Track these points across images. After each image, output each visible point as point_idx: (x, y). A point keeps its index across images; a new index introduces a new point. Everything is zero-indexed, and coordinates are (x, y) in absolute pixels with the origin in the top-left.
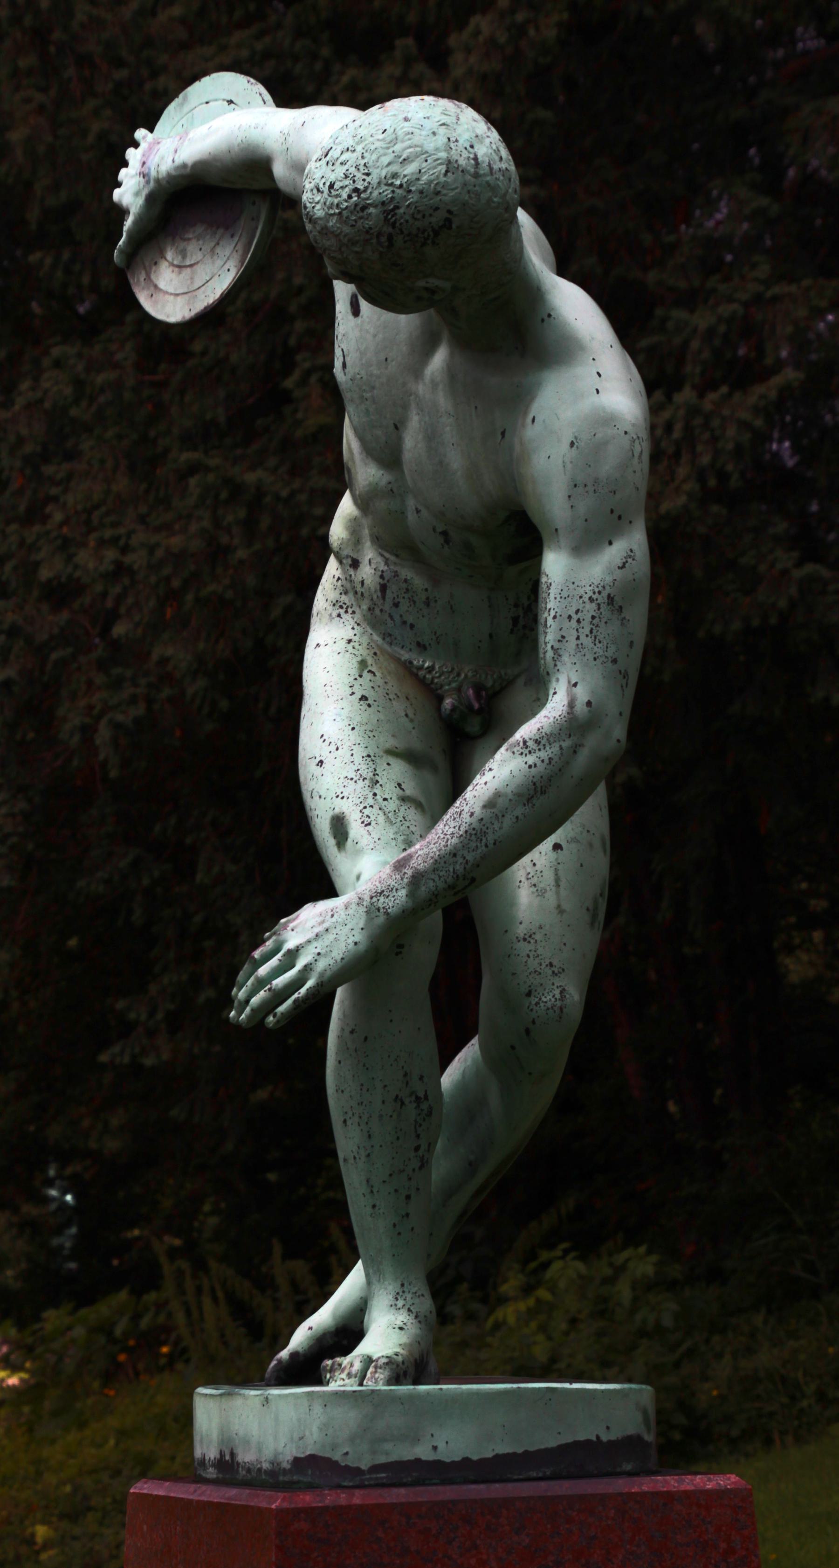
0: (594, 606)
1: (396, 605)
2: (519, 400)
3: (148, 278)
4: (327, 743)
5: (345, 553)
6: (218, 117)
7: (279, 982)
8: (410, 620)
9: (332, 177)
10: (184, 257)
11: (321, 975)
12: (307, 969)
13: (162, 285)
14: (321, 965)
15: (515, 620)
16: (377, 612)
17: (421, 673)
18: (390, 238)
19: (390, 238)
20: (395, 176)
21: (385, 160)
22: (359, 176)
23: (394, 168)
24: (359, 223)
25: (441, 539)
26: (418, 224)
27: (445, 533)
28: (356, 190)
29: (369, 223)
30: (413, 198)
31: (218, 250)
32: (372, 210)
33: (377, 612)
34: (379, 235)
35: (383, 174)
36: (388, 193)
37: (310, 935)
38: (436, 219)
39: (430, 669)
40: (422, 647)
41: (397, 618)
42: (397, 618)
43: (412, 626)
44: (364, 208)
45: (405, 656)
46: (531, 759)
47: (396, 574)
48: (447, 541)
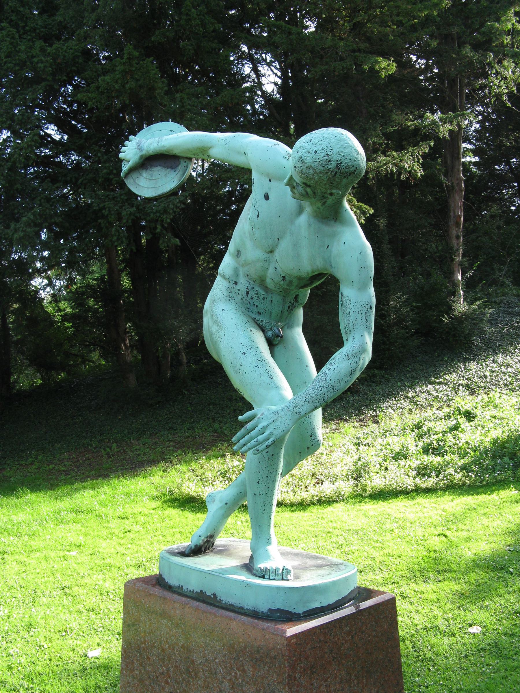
0: (366, 309)
1: (252, 299)
2: (334, 235)
3: (134, 181)
4: (245, 346)
5: (231, 279)
6: (166, 135)
7: (261, 438)
8: (257, 304)
9: (316, 149)
10: (152, 176)
11: (276, 436)
12: (271, 434)
13: (141, 184)
14: (276, 432)
15: (289, 307)
16: (244, 300)
17: (258, 322)
18: (336, 173)
19: (336, 173)
20: (342, 152)
21: (338, 146)
22: (328, 150)
23: (341, 149)
24: (326, 166)
25: (282, 279)
26: (347, 170)
27: (284, 277)
28: (327, 154)
29: (330, 167)
30: (347, 161)
31: (168, 175)
32: (332, 162)
33: (244, 300)
34: (332, 171)
35: (338, 150)
36: (339, 158)
37: (270, 421)
38: (352, 170)
39: (262, 321)
40: (259, 313)
41: (252, 303)
42: (252, 303)
43: (257, 306)
44: (329, 161)
45: (253, 316)
46: (351, 361)
47: (253, 288)
48: (283, 280)
